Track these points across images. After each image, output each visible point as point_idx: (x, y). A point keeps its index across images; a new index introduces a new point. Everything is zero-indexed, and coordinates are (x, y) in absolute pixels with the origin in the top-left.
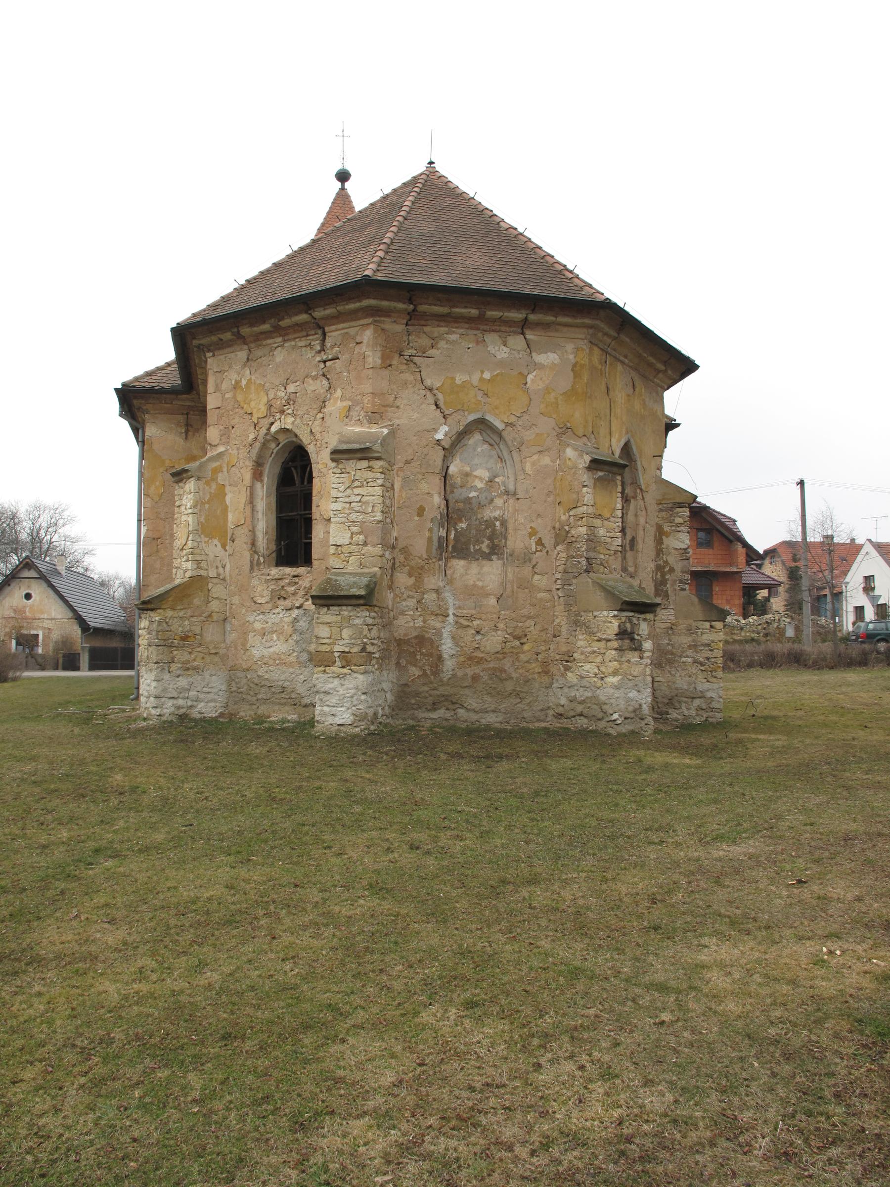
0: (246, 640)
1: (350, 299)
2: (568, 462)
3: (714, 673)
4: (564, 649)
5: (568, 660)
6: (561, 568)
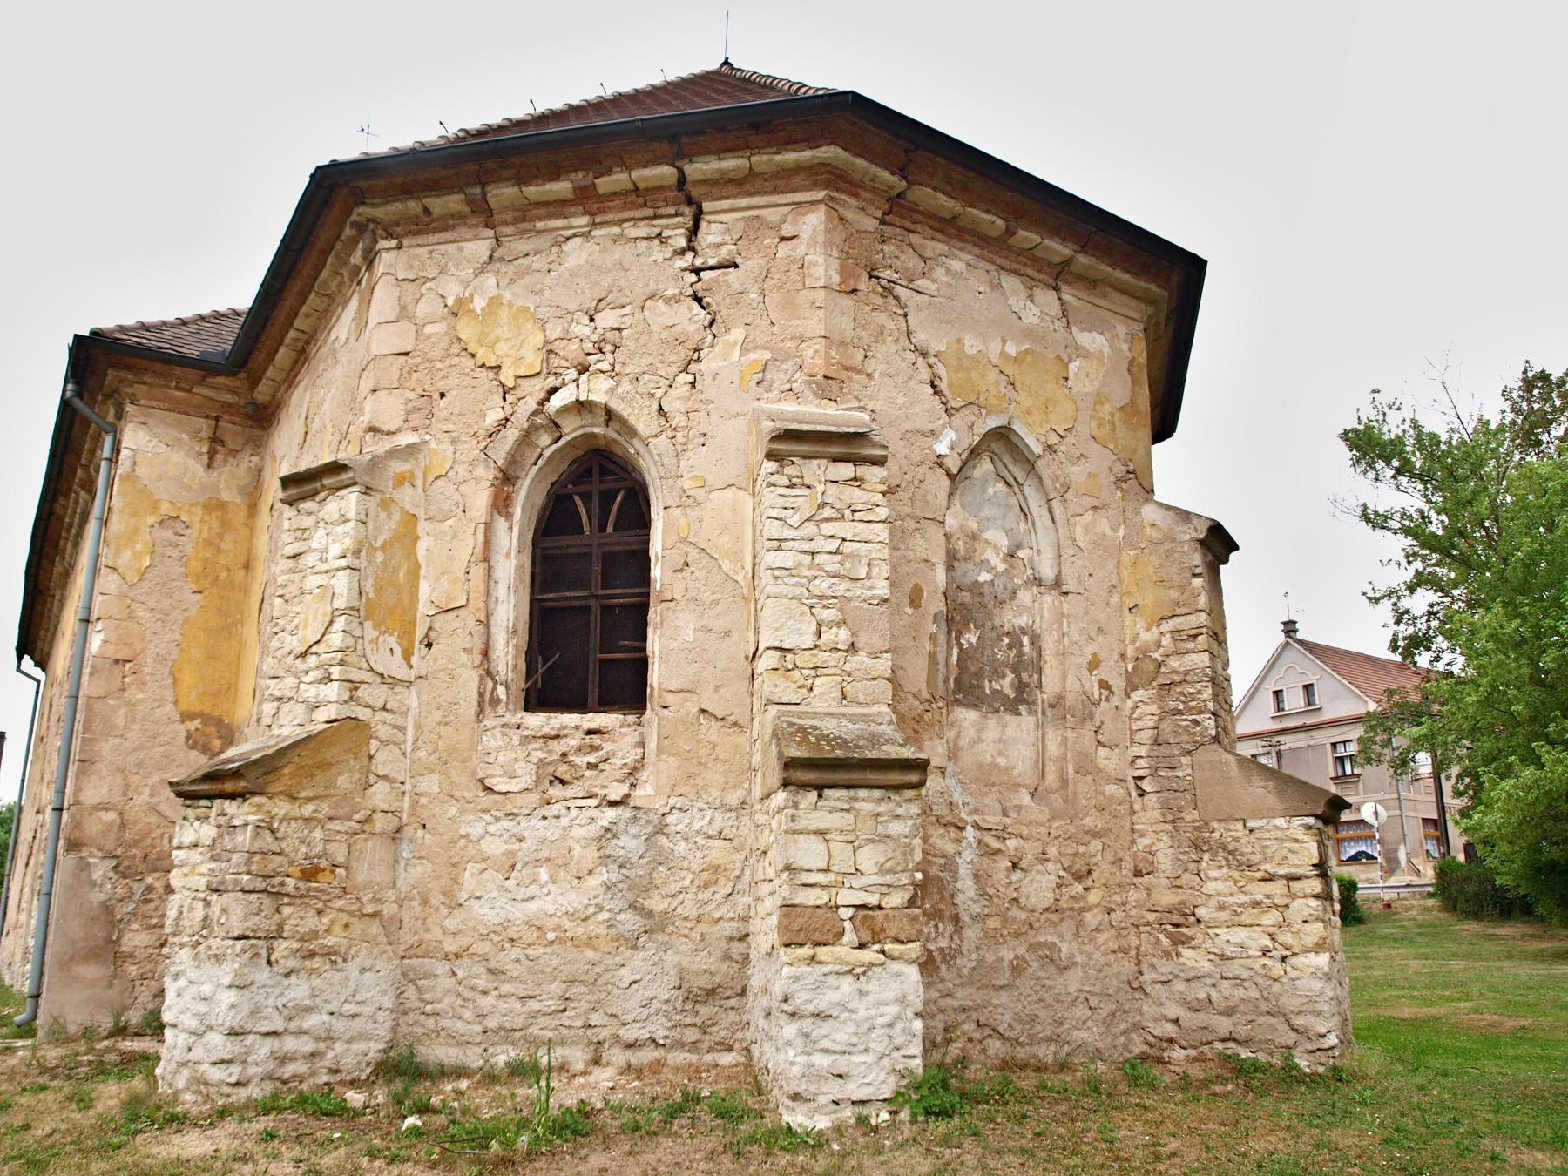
4: (1168, 898)
6: (1146, 736)
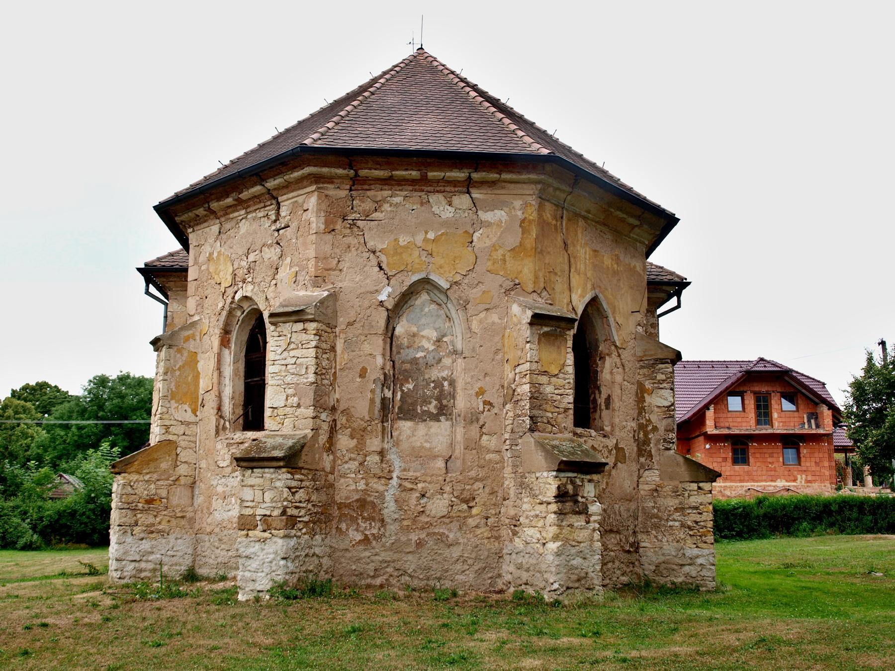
0: (210, 503)
1: (294, 168)
2: (515, 319)
3: (704, 538)
5: (515, 523)
6: (509, 428)
